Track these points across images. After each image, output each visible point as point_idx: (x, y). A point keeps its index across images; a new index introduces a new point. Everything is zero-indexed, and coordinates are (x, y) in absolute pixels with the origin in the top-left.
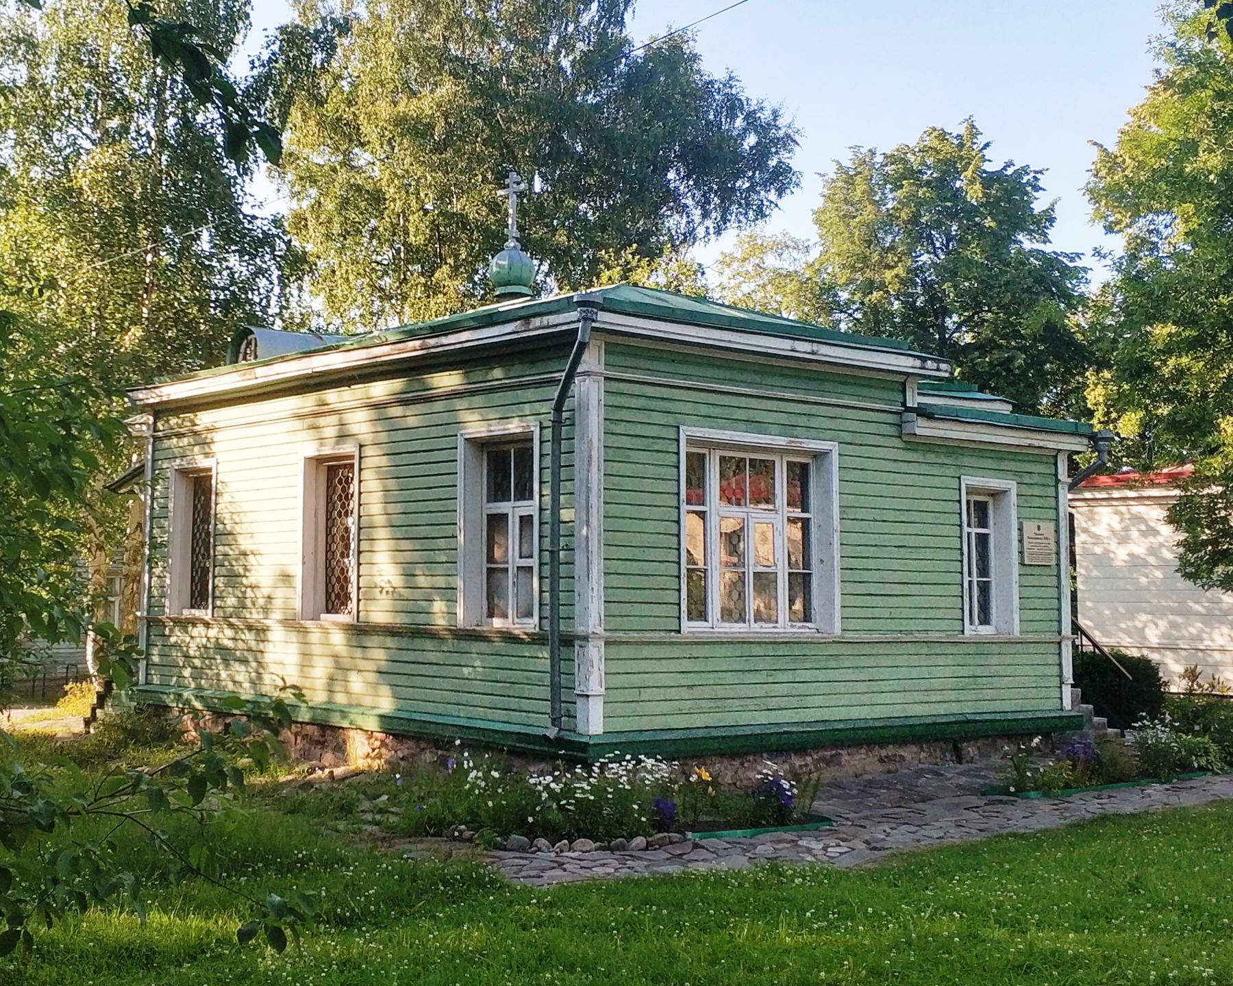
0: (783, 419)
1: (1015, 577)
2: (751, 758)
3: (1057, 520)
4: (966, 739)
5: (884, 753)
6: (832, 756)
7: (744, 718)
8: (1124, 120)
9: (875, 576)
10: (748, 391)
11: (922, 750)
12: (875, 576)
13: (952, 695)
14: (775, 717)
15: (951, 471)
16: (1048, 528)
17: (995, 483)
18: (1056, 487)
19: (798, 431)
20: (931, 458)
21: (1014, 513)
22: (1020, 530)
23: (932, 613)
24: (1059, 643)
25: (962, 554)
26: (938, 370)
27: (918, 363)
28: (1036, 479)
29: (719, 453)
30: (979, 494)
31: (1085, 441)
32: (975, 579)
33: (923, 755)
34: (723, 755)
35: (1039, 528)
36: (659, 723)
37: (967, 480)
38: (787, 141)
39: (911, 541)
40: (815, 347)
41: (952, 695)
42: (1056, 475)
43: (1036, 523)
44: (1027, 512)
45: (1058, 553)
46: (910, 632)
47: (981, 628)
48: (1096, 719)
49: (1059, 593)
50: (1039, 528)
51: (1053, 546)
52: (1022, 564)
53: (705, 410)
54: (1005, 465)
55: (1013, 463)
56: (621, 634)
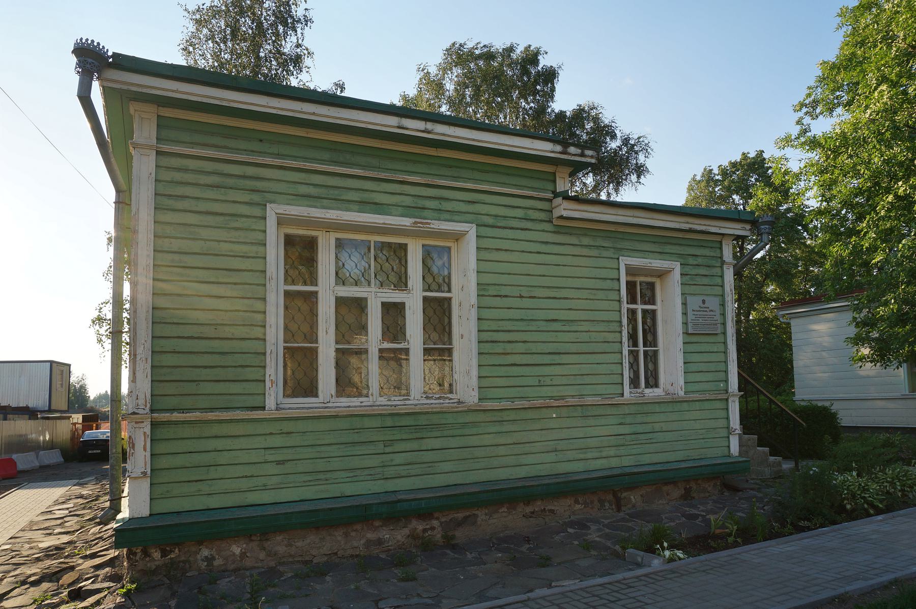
0: (408, 201)
1: (680, 344)
2: (358, 527)
3: (723, 296)
4: (631, 488)
5: (528, 510)
6: (466, 518)
7: (350, 489)
8: (837, 52)
9: (520, 347)
10: (360, 172)
11: (577, 502)
12: (520, 347)
13: (612, 452)
14: (391, 486)
15: (609, 253)
16: (713, 303)
17: (657, 264)
18: (722, 267)
19: (426, 213)
20: (586, 241)
21: (678, 290)
22: (684, 304)
23: (587, 380)
24: (727, 400)
25: (621, 326)
26: (582, 155)
27: (559, 148)
28: (700, 261)
29: (333, 236)
30: (646, 276)
31: (748, 227)
32: (641, 348)
33: (578, 507)
34: (317, 528)
35: (704, 302)
36: (229, 501)
37: (624, 261)
38: (709, 173)
39: (563, 315)
40: (430, 126)
41: (612, 452)
42: (721, 257)
43: (702, 298)
44: (688, 289)
45: (724, 324)
46: (562, 398)
47: (648, 391)
48: (772, 458)
49: (726, 358)
50: (704, 302)
51: (719, 318)
52: (686, 333)
53: (303, 189)
54: (668, 249)
55: (677, 247)
56: (198, 414)
